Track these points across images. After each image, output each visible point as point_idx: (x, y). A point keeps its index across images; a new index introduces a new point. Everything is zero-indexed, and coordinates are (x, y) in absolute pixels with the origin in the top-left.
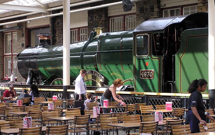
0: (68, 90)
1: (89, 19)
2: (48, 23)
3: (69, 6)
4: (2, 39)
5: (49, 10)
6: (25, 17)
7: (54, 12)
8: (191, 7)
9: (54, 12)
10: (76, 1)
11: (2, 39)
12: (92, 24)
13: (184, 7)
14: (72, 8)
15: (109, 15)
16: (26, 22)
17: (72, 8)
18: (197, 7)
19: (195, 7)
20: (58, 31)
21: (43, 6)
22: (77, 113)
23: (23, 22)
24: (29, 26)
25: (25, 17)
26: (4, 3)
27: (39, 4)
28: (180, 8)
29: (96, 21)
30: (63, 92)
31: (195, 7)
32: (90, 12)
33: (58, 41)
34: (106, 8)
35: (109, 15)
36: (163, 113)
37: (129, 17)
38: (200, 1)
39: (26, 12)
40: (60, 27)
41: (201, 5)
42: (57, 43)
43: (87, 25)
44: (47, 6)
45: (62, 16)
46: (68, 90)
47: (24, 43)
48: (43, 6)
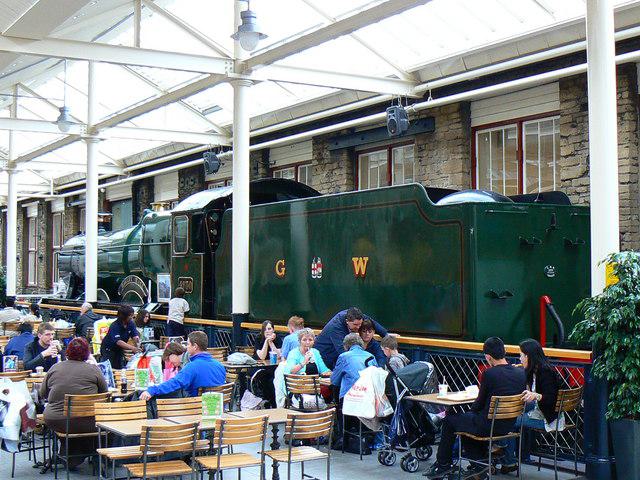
0: (243, 325)
2: (129, 194)
3: (609, 37)
4: (352, 174)
5: (125, 170)
7: (135, 172)
9: (135, 172)
10: (280, 121)
11: (352, 174)
14: (101, 182)
15: (475, 123)
21: (403, 79)
26: (35, 159)
30: (230, 328)
32: (182, 173)
34: (152, 178)
35: (475, 123)
41: (315, 162)
44: (124, 163)
45: (583, 76)
46: (243, 325)
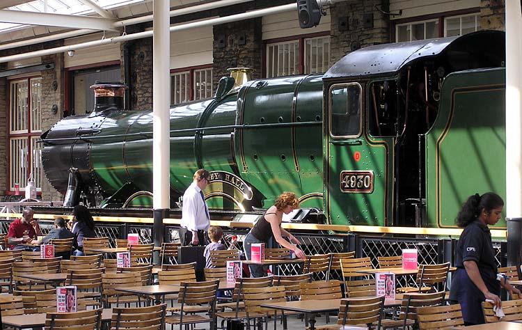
0: (166, 221)
1: (217, 46)
2: (116, 56)
3: (167, 14)
4: (5, 95)
5: (119, 23)
6: (61, 42)
7: (131, 29)
8: (463, 18)
9: (131, 29)
10: (184, 3)
11: (5, 95)
12: (223, 58)
14: (175, 20)
15: (265, 37)
16: (63, 54)
17: (175, 20)
18: (478, 16)
19: (472, 18)
21: (103, 16)
22: (186, 277)
23: (55, 55)
24: (71, 64)
25: (61, 42)
26: (11, 8)
27: (94, 10)
29: (234, 51)
30: (152, 224)
32: (218, 29)
34: (258, 19)
35: (265, 37)
37: (313, 41)
38: (486, 3)
39: (62, 29)
41: (488, 11)
42: (138, 104)
43: (210, 60)
44: (115, 15)
45: (150, 39)
46: (166, 221)
47: (59, 105)
48: (103, 16)
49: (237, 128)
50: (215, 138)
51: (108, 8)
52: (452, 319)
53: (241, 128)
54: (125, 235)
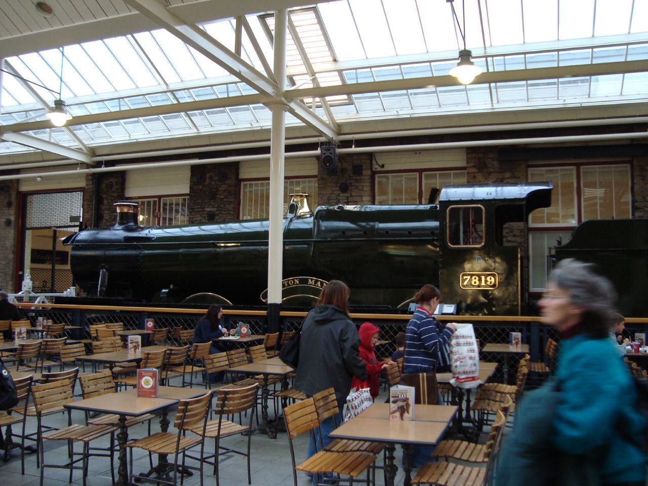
1: (195, 180)
3: (284, 142)
6: (17, 171)
8: (392, 176)
12: (200, 190)
13: (164, 198)
15: (242, 176)
16: (18, 181)
17: (288, 148)
18: (439, 174)
19: (450, 174)
20: (107, 200)
22: (79, 354)
23: (11, 181)
24: (24, 188)
25: (17, 171)
27: (81, 146)
28: (157, 199)
29: (213, 185)
31: (450, 174)
32: (194, 168)
33: (107, 218)
35: (242, 176)
36: (166, 385)
37: (290, 182)
38: (472, 164)
39: (63, 158)
40: (113, 192)
42: (104, 221)
43: (186, 190)
44: (93, 151)
47: (12, 218)
48: (85, 151)
49: (315, 242)
50: (253, 250)
51: (90, 146)
52: (105, 389)
53: (319, 242)
54: (467, 317)
